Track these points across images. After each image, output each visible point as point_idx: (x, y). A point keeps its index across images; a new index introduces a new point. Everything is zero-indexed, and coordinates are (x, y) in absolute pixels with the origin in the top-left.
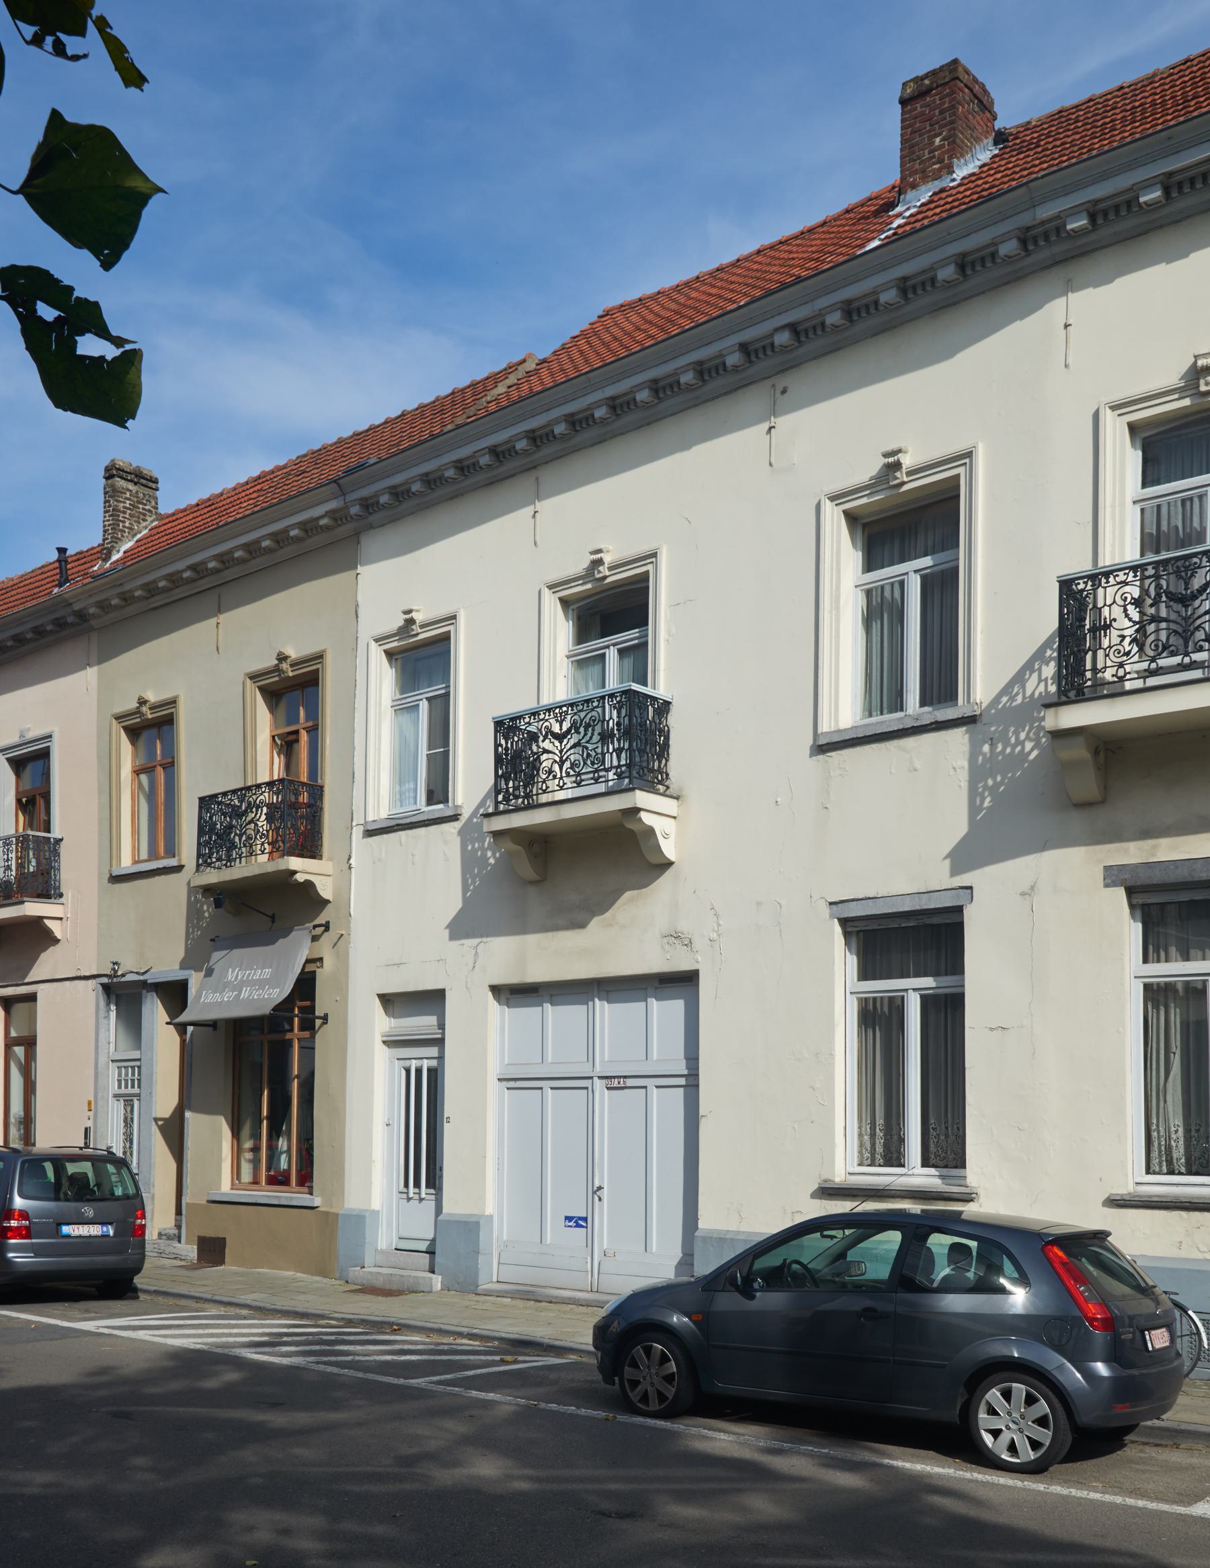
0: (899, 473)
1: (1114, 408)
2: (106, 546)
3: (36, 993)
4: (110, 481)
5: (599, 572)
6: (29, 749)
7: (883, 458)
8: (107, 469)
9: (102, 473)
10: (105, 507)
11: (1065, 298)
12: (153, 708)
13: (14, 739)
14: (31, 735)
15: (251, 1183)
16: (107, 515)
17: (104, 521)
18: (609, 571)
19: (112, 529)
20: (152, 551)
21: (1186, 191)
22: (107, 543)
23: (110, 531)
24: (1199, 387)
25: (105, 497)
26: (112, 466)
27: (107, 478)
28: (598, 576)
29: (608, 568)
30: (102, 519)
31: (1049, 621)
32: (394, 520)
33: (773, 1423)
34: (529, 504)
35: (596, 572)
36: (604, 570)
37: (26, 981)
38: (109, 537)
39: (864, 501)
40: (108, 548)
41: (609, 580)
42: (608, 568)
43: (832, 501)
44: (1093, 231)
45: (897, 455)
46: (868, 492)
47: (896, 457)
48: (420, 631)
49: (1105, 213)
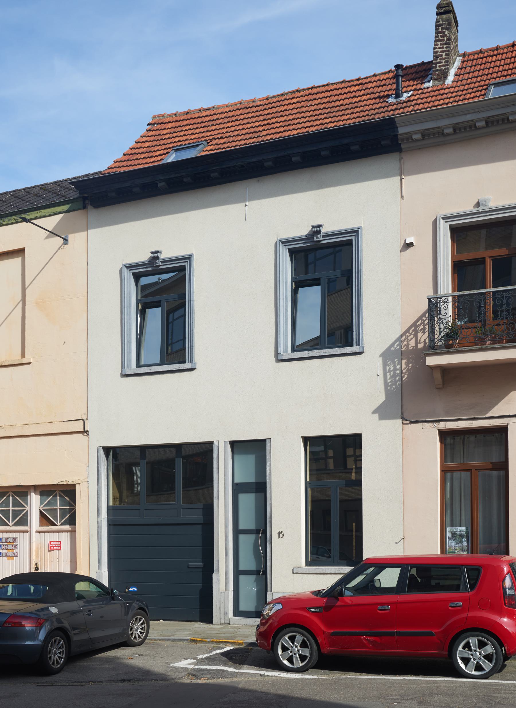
0: (319, 235)
1: (443, 218)
2: (438, 68)
3: (507, 426)
4: (444, 16)
5: (317, 238)
6: (489, 217)
7: (151, 254)
8: (439, 6)
9: (435, 10)
10: (436, 37)
11: (86, 232)
12: (164, 261)
13: (469, 208)
14: (492, 204)
15: (73, 532)
16: (439, 43)
17: (435, 49)
18: (323, 238)
19: (446, 55)
20: (154, 162)
21: (462, 131)
22: (440, 66)
23: (444, 57)
24: (314, 239)
25: (437, 29)
26: (447, 4)
27: (438, 14)
28: (315, 239)
29: (323, 236)
30: (433, 47)
31: (425, 306)
32: (420, 148)
33: (390, 675)
34: (245, 202)
35: (315, 237)
36: (320, 237)
37: (488, 415)
38: (443, 61)
39: (302, 245)
40: (440, 70)
41: (161, 267)
42: (323, 236)
43: (283, 244)
44: (454, 134)
45: (319, 227)
46: (304, 242)
47: (156, 254)
48: (322, 239)
49: (460, 129)
